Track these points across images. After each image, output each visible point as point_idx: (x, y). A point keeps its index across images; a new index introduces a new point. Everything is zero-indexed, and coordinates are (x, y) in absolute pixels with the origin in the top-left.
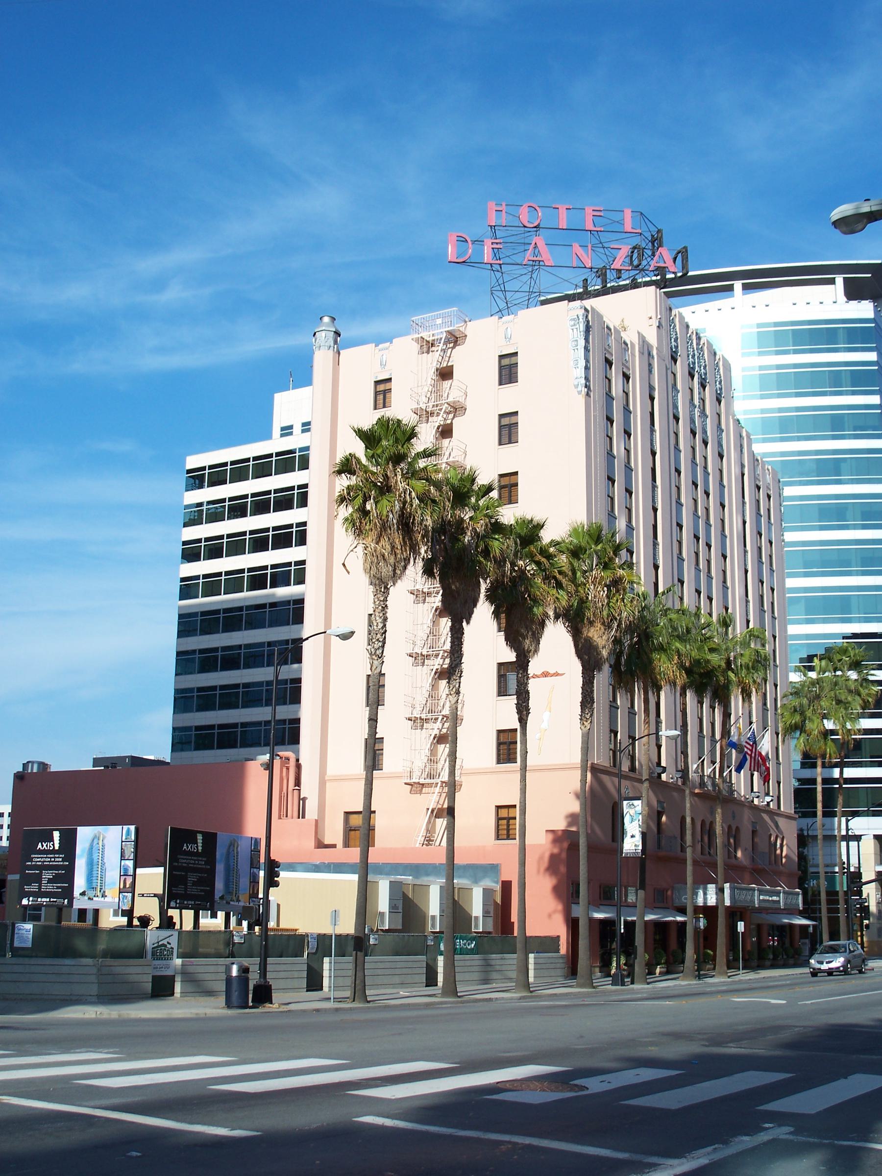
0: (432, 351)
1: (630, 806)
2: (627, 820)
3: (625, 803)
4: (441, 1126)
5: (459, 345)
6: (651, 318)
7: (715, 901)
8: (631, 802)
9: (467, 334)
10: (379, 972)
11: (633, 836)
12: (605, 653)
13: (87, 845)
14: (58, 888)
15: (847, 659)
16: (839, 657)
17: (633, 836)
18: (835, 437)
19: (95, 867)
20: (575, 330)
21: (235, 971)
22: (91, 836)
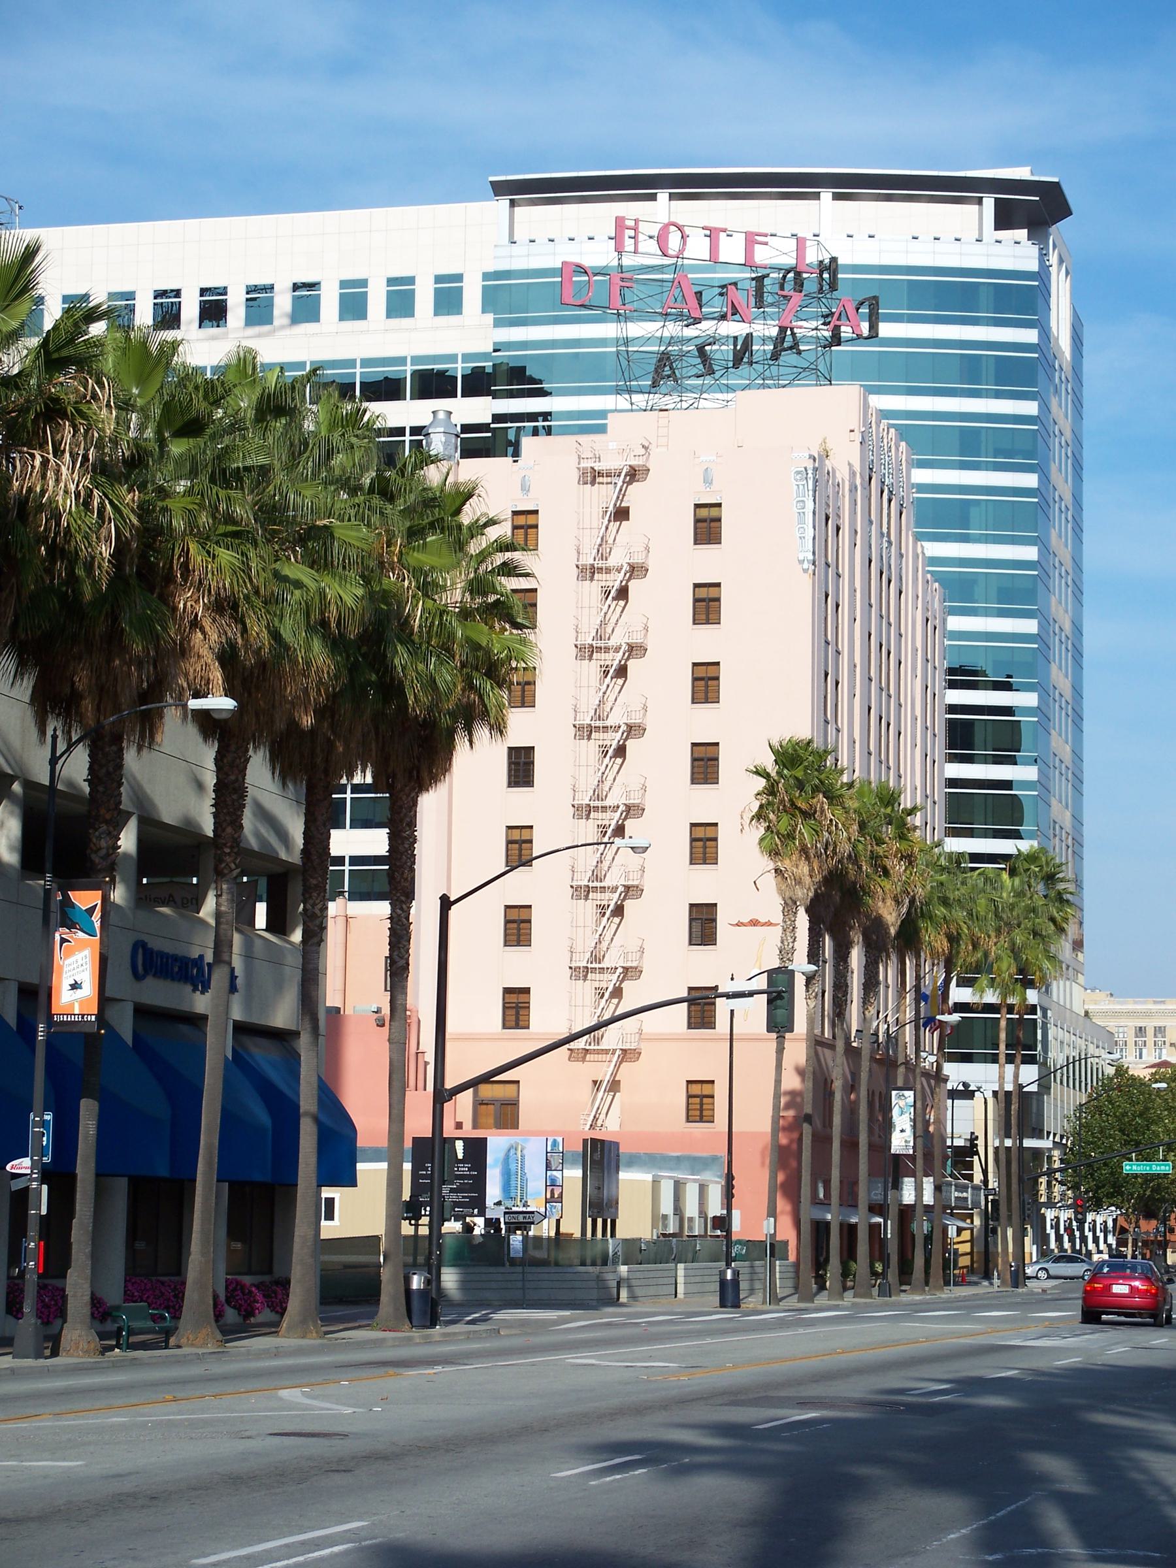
0: (599, 483)
1: (899, 1097)
2: (895, 1112)
3: (894, 1093)
4: (632, 1455)
5: (638, 481)
6: (852, 431)
7: (914, 1198)
8: (901, 1093)
9: (650, 466)
10: (661, 1281)
11: (902, 1131)
12: (893, 931)
13: (501, 1155)
14: (464, 1197)
15: (1037, 869)
16: (1026, 866)
17: (902, 1131)
18: (964, 466)
19: (513, 1177)
20: (801, 487)
21: (729, 1275)
22: (506, 1146)
